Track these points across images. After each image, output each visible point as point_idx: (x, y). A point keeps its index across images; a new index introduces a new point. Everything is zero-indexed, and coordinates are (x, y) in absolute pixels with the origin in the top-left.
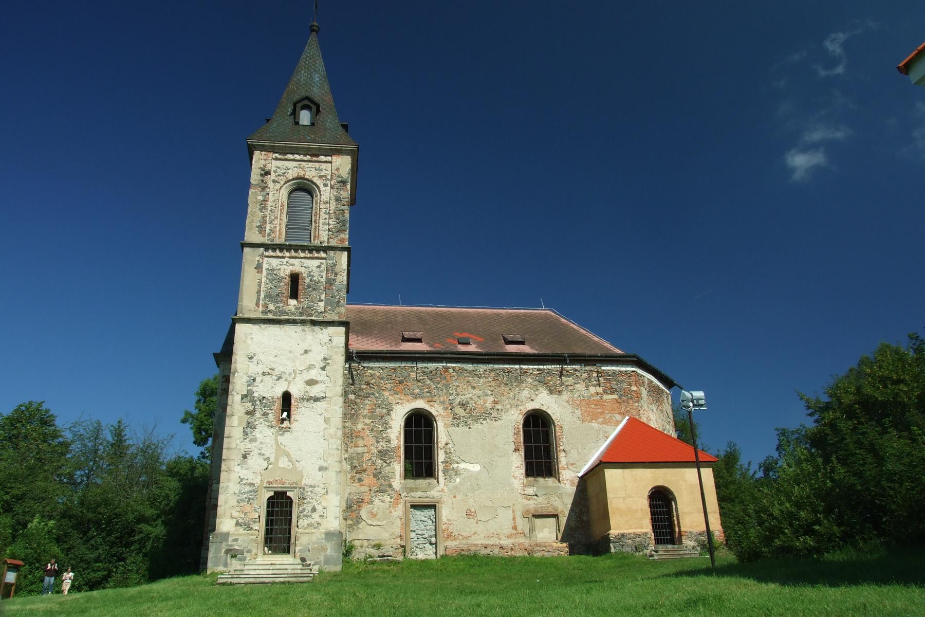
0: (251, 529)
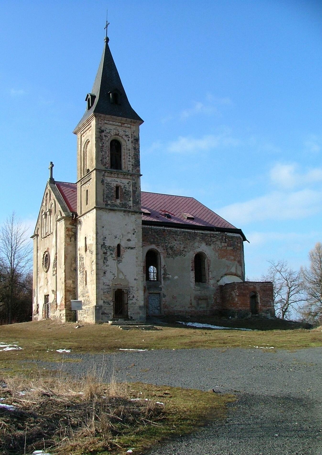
0: (110, 304)
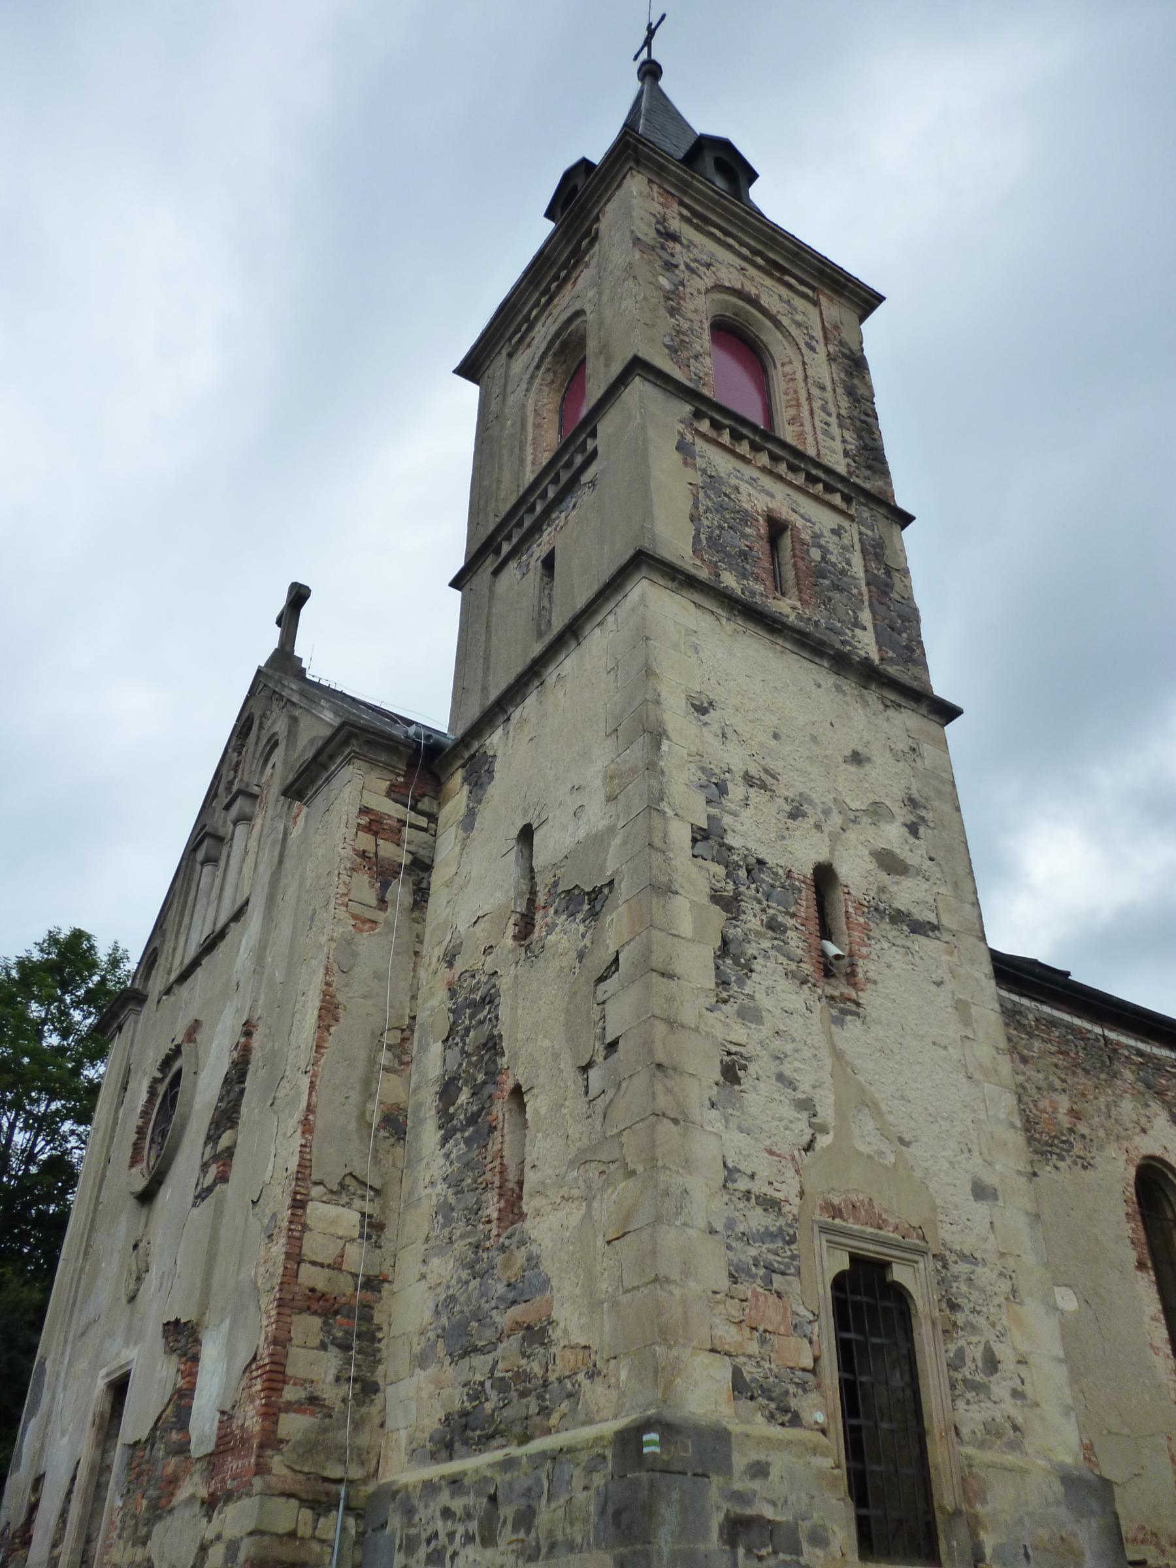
0: (796, 1420)
